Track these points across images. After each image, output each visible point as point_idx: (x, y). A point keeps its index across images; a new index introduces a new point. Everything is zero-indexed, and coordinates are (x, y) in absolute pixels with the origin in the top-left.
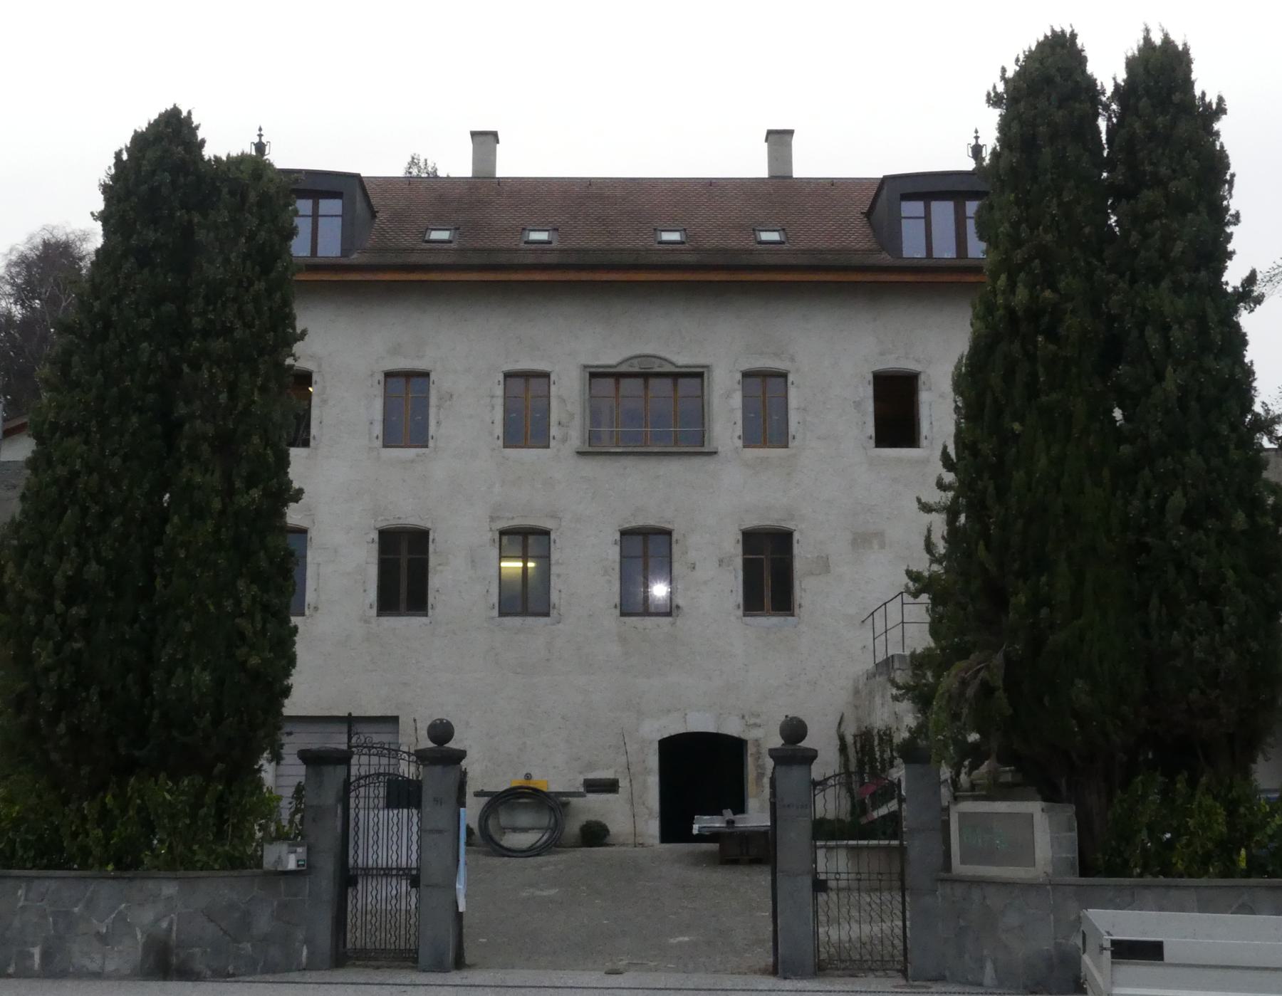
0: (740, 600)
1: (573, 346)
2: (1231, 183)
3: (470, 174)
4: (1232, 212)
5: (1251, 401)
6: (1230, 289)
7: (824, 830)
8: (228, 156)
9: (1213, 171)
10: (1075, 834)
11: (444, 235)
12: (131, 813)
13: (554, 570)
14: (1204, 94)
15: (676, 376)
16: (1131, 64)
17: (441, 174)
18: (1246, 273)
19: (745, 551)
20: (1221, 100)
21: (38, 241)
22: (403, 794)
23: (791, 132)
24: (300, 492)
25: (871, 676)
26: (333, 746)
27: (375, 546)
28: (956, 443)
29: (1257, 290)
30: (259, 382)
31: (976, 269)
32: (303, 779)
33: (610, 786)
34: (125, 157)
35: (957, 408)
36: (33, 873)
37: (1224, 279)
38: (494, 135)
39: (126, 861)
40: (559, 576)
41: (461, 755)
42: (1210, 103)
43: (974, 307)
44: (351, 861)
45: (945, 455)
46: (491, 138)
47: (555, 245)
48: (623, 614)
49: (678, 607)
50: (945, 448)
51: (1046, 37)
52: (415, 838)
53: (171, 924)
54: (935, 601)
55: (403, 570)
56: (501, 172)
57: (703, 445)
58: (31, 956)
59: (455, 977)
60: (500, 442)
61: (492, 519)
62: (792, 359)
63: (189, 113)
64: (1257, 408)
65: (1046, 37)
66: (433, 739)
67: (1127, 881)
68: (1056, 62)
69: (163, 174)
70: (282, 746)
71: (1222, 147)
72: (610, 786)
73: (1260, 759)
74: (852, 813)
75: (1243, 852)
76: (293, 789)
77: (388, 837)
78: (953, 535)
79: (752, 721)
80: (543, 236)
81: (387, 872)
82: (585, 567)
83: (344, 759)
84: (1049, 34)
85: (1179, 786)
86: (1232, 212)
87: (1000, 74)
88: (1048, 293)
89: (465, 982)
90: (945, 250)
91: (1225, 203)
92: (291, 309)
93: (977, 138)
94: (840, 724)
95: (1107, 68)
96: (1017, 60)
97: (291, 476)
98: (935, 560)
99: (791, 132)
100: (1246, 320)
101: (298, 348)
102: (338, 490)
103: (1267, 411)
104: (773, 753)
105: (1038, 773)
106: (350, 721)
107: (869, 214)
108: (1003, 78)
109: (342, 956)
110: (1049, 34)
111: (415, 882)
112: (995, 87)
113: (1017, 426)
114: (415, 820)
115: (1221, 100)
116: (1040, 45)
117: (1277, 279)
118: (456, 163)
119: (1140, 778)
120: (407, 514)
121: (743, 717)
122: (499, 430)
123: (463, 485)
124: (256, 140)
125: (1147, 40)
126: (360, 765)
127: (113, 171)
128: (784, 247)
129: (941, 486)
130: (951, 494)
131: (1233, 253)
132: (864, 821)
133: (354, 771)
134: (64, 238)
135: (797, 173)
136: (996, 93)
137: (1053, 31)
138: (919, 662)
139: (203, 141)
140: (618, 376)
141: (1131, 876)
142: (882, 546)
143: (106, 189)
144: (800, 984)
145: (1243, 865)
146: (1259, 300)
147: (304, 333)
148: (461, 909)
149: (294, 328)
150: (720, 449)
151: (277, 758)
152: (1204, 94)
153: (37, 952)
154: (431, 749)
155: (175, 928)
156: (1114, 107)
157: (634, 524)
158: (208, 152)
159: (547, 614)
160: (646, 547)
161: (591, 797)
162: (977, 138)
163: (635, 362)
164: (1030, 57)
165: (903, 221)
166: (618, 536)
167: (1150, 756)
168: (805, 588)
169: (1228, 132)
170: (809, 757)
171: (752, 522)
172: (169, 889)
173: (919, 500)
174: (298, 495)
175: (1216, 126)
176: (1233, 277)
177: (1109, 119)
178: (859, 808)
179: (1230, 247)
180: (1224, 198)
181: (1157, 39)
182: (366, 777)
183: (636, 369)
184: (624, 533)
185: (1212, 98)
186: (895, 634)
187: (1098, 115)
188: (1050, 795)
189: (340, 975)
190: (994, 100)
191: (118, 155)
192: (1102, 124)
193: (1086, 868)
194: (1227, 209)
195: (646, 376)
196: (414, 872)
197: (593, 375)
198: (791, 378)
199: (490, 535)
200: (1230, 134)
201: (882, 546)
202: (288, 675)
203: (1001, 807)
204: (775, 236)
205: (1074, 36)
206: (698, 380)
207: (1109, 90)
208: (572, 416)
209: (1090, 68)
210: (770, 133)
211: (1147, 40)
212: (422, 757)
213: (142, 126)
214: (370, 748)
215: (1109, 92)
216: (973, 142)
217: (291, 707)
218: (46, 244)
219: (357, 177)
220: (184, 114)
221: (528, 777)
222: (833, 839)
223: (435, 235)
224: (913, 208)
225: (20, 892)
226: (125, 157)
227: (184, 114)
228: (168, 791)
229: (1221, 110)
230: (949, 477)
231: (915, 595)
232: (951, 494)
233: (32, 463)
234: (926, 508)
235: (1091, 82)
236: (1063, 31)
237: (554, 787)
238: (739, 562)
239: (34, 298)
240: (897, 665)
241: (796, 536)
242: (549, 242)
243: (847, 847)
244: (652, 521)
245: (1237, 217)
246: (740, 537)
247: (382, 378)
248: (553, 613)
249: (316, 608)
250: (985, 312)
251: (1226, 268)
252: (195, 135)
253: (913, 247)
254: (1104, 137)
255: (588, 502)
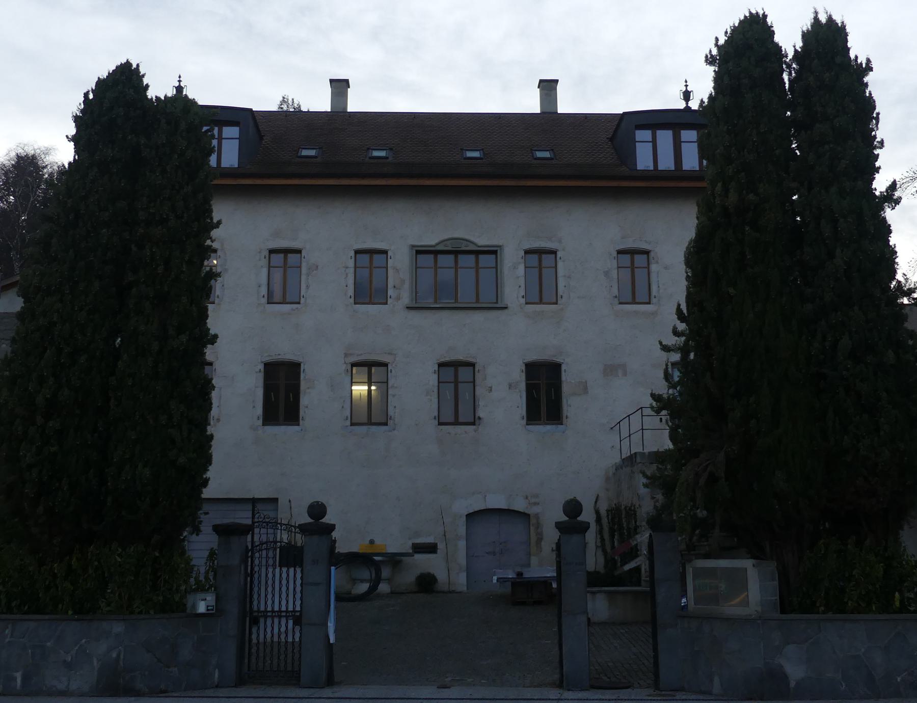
0: (524, 413)
1: (403, 229)
2: (877, 119)
3: (537, 110)
4: (878, 139)
5: (894, 272)
6: (877, 193)
7: (595, 580)
8: (166, 96)
9: (864, 111)
10: (776, 583)
11: (312, 153)
12: (90, 571)
13: (390, 392)
14: (856, 57)
15: (477, 253)
16: (805, 36)
17: (304, 109)
18: (888, 183)
19: (528, 378)
20: (868, 61)
21: (13, 154)
22: (291, 557)
23: (556, 81)
24: (216, 337)
25: (618, 468)
26: (232, 520)
27: (261, 375)
28: (687, 302)
29: (897, 194)
30: (187, 258)
31: (691, 176)
32: (215, 547)
33: (431, 549)
34: (91, 96)
35: (688, 276)
36: (18, 616)
37: (873, 187)
38: (346, 82)
39: (85, 608)
40: (394, 396)
41: (332, 527)
42: (861, 64)
43: (698, 205)
44: (255, 608)
45: (679, 311)
46: (344, 83)
47: (390, 159)
48: (440, 424)
49: (479, 418)
50: (679, 305)
51: (745, 17)
52: (298, 589)
53: (119, 655)
54: (672, 416)
55: (282, 392)
56: (351, 108)
57: (497, 303)
58: (15, 679)
59: (328, 692)
60: (352, 300)
61: (346, 355)
62: (560, 241)
63: (138, 65)
64: (899, 277)
65: (745, 17)
66: (310, 516)
67: (816, 616)
68: (752, 35)
69: (118, 107)
70: (201, 522)
71: (870, 94)
72: (431, 549)
73: (906, 527)
74: (605, 567)
75: (897, 595)
76: (207, 553)
77: (280, 590)
78: (683, 364)
79: (533, 500)
80: (382, 154)
81: (279, 614)
82: (416, 391)
83: (246, 530)
84: (748, 15)
85: (849, 546)
86: (878, 139)
87: (714, 42)
88: (751, 197)
89: (336, 695)
90: (666, 163)
91: (873, 133)
92: (210, 206)
93: (686, 86)
94: (596, 502)
95: (789, 38)
96: (726, 32)
97: (209, 326)
98: (672, 386)
99: (556, 81)
100: (890, 214)
101: (215, 233)
102: (239, 335)
103: (907, 280)
104: (559, 525)
105: (748, 539)
106: (254, 501)
107: (611, 139)
108: (716, 45)
109: (245, 677)
110: (748, 15)
111: (298, 621)
112: (710, 51)
113: (731, 291)
114: (299, 575)
115: (868, 61)
116: (741, 22)
117: (906, 185)
118: (319, 101)
119: (822, 541)
120: (285, 351)
121: (527, 498)
122: (351, 292)
123: (323, 329)
124: (177, 84)
125: (816, 19)
126: (260, 535)
127: (83, 106)
128: (554, 162)
129: (676, 333)
130: (683, 339)
131: (879, 168)
132: (617, 573)
133: (256, 538)
134: (33, 152)
135: (349, 110)
136: (712, 55)
137: (750, 13)
138: (658, 457)
139: (147, 86)
140: (436, 253)
141: (818, 613)
142: (625, 374)
143: (76, 119)
144: (580, 695)
145: (897, 604)
146: (898, 201)
147: (219, 223)
148: (331, 642)
149: (212, 219)
150: (509, 305)
151: (197, 530)
152: (856, 57)
153: (19, 676)
154: (309, 523)
155: (122, 657)
156: (794, 66)
157: (447, 359)
158: (151, 94)
159: (386, 424)
160: (457, 373)
161: (418, 557)
162: (686, 86)
163: (448, 243)
164: (735, 30)
165: (637, 144)
166: (436, 368)
167: (827, 525)
168: (571, 405)
169: (875, 83)
170: (583, 528)
171: (533, 357)
172: (118, 628)
173: (661, 343)
174: (214, 339)
175: (865, 80)
176: (880, 184)
177: (790, 74)
178: (610, 563)
179: (877, 164)
180: (873, 130)
181: (823, 18)
182: (266, 543)
183: (449, 248)
184: (441, 365)
185: (862, 60)
186: (636, 438)
187: (783, 71)
188: (757, 554)
189: (243, 691)
190: (710, 60)
191: (86, 95)
192: (786, 77)
193: (785, 606)
194: (875, 137)
195: (456, 253)
196: (298, 614)
197: (418, 252)
198: (559, 254)
199: (344, 367)
200: (876, 85)
201: (625, 374)
202: (206, 470)
203: (723, 563)
204: (547, 154)
205: (765, 16)
206: (494, 256)
207: (791, 54)
208: (403, 282)
209: (777, 39)
210: (541, 81)
211: (816, 19)
212: (303, 529)
213: (104, 75)
214: (267, 523)
215: (790, 56)
216: (684, 89)
217: (207, 493)
218: (19, 157)
219: (251, 110)
220: (134, 66)
221: (372, 542)
222: (595, 586)
223: (305, 153)
224: (643, 135)
225: (7, 632)
226: (91, 96)
227: (134, 66)
228: (119, 555)
229: (869, 68)
230: (682, 327)
231: (658, 411)
232: (683, 339)
233: (20, 316)
234: (666, 348)
235: (778, 48)
236: (757, 13)
237: (391, 550)
238: (523, 386)
239: (9, 195)
240: (638, 460)
241: (563, 367)
242: (386, 158)
243: (605, 592)
244: (461, 357)
245: (882, 143)
246: (524, 368)
247: (267, 253)
248: (390, 422)
249: (218, 420)
250: (706, 210)
251: (874, 178)
252: (142, 81)
253: (644, 161)
254: (787, 86)
255: (418, 341)
